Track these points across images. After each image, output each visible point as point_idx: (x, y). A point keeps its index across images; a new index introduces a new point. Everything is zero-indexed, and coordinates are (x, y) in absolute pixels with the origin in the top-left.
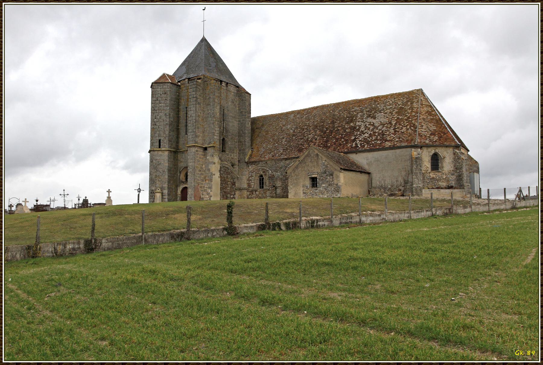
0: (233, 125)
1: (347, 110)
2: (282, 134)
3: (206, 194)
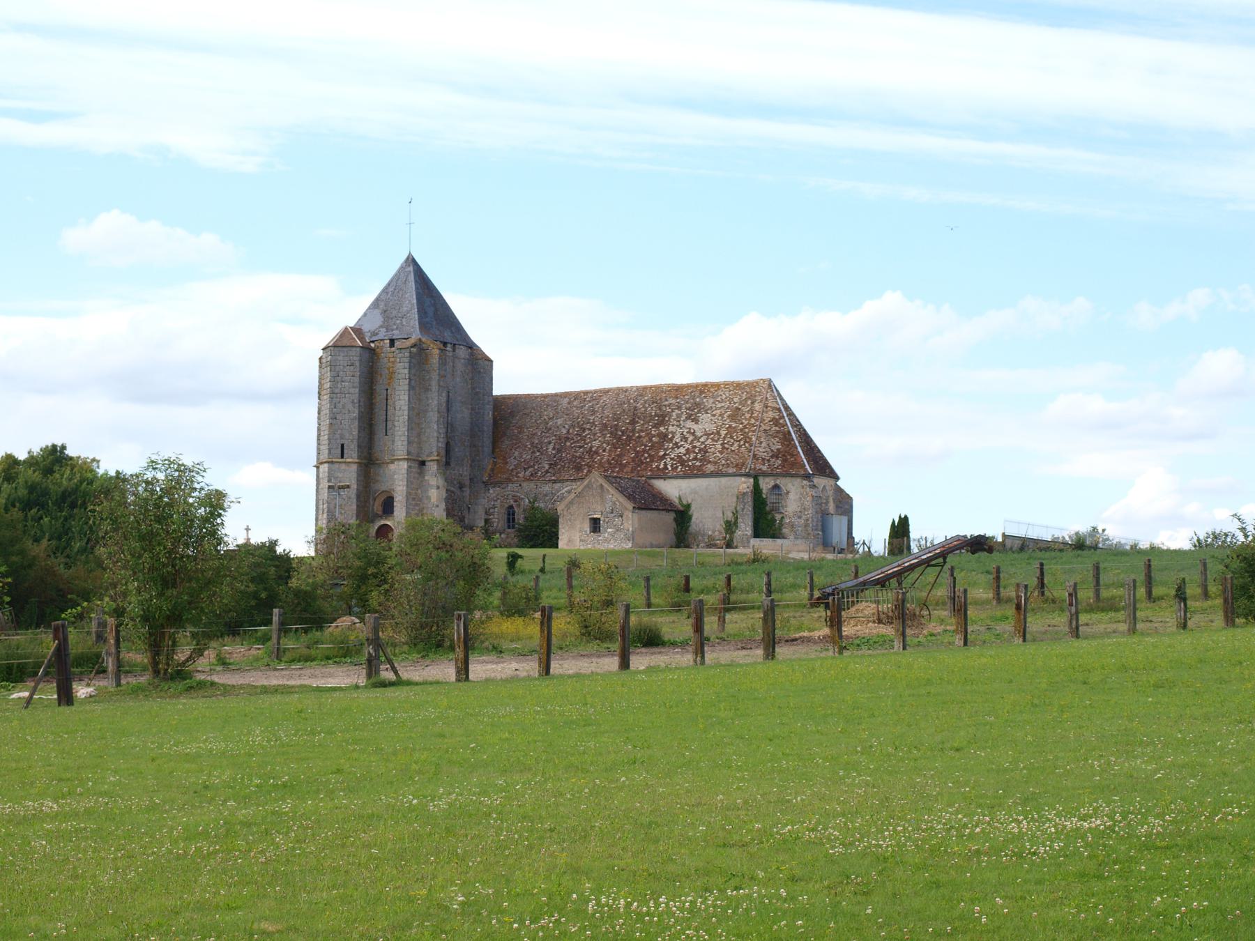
0: (462, 415)
1: (656, 402)
2: (548, 435)
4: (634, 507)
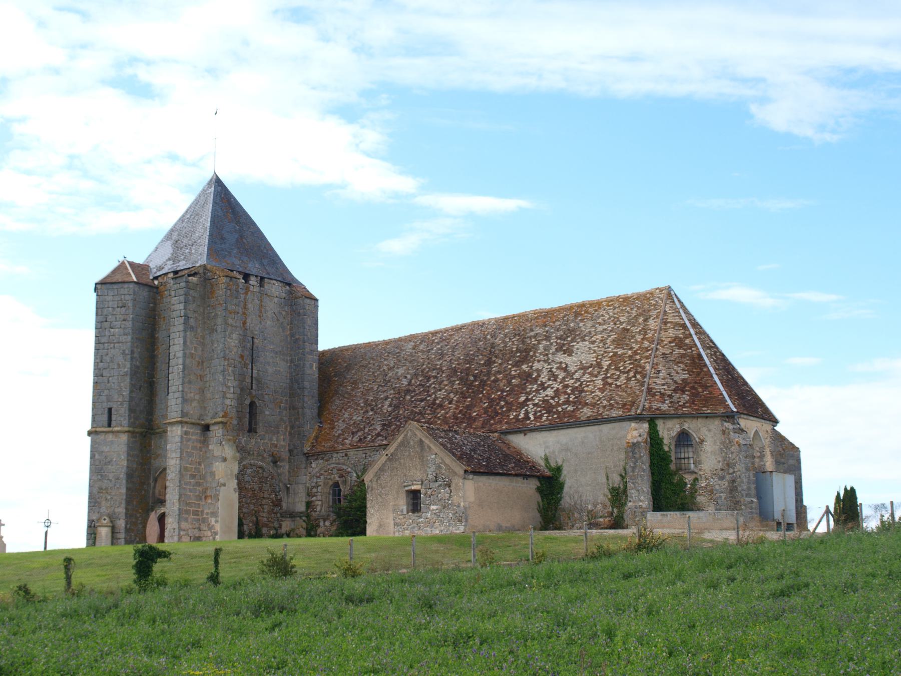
1: (519, 335)
2: (385, 388)
3: (207, 529)
4: (466, 471)
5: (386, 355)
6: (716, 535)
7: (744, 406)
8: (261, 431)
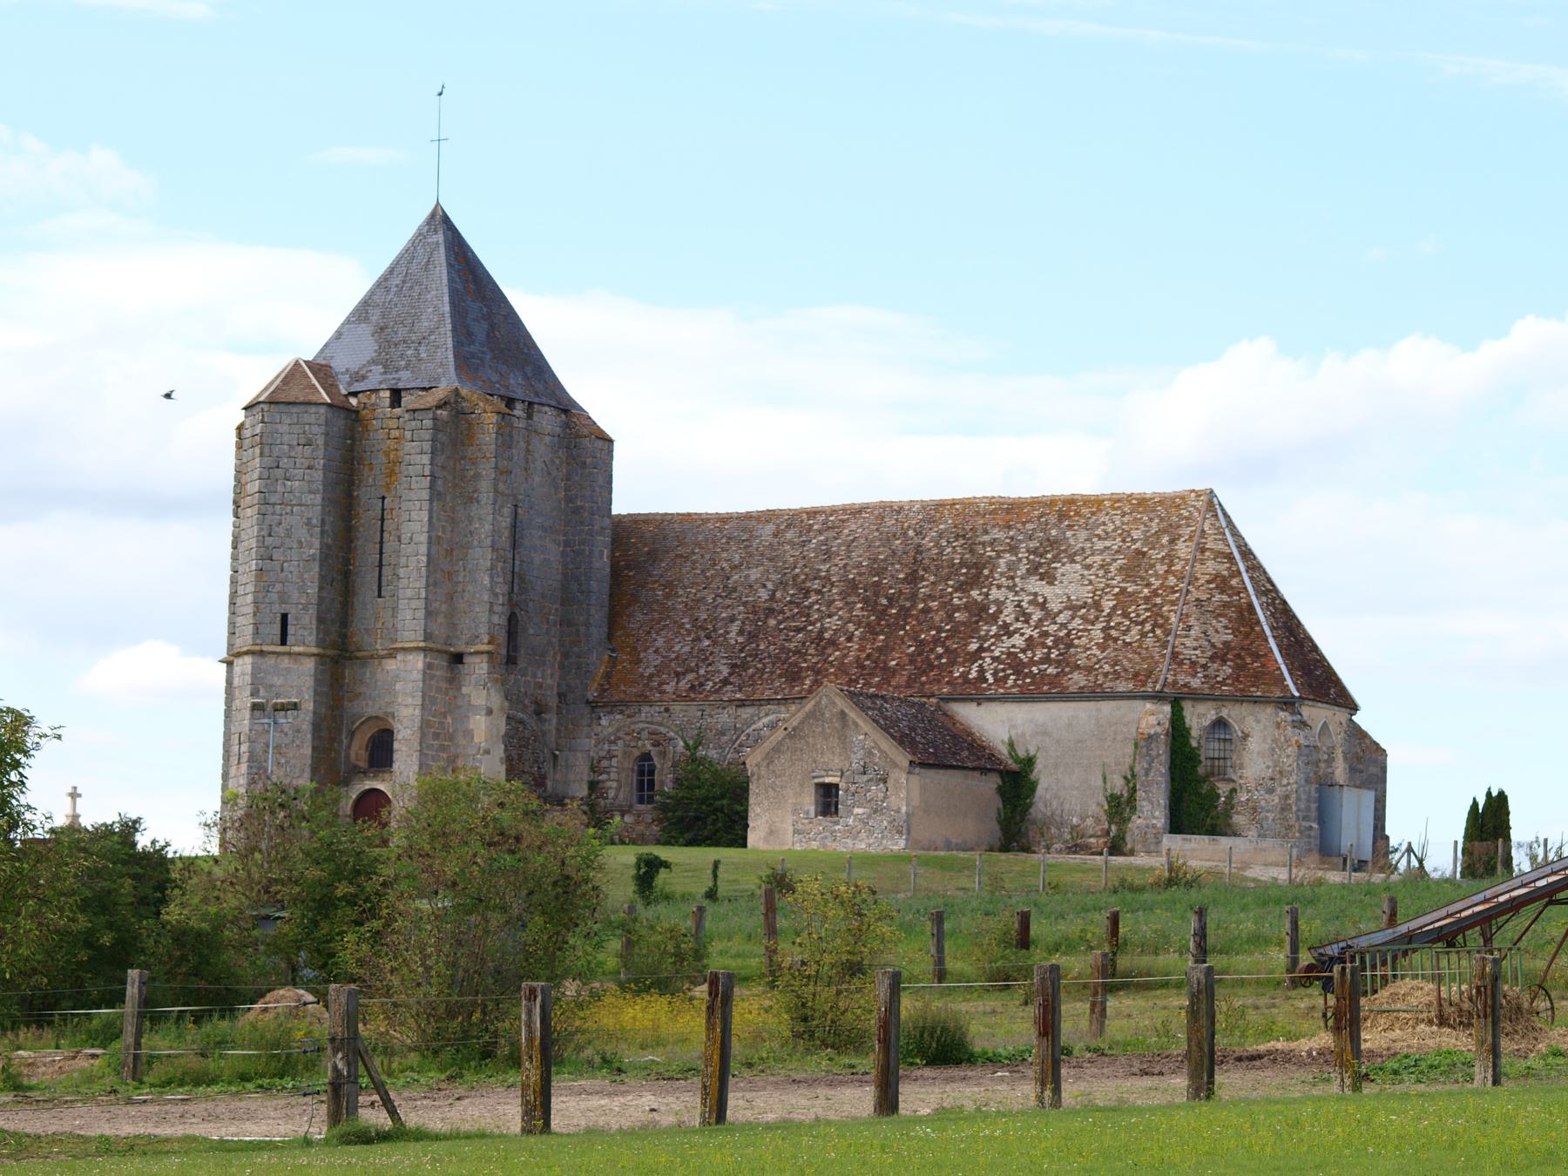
1: (964, 536)
2: (728, 602)
5: (724, 541)
6: (1257, 872)
7: (1310, 686)
8: (522, 663)
